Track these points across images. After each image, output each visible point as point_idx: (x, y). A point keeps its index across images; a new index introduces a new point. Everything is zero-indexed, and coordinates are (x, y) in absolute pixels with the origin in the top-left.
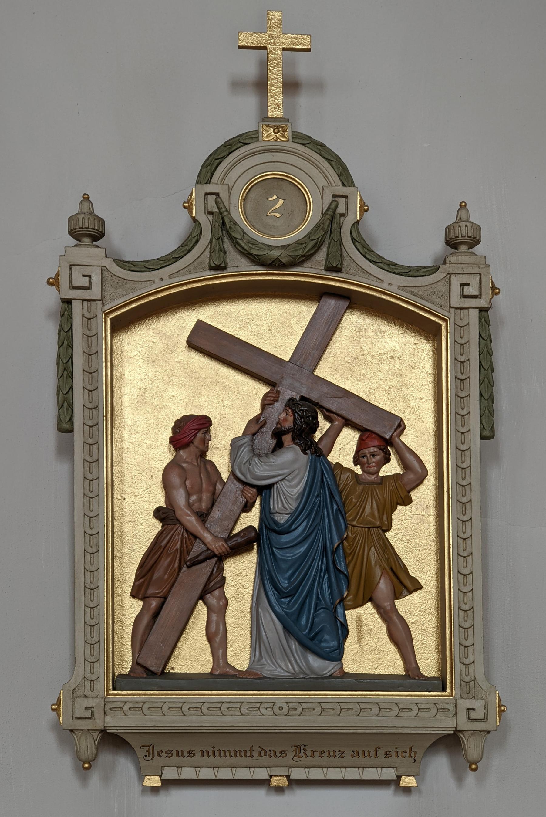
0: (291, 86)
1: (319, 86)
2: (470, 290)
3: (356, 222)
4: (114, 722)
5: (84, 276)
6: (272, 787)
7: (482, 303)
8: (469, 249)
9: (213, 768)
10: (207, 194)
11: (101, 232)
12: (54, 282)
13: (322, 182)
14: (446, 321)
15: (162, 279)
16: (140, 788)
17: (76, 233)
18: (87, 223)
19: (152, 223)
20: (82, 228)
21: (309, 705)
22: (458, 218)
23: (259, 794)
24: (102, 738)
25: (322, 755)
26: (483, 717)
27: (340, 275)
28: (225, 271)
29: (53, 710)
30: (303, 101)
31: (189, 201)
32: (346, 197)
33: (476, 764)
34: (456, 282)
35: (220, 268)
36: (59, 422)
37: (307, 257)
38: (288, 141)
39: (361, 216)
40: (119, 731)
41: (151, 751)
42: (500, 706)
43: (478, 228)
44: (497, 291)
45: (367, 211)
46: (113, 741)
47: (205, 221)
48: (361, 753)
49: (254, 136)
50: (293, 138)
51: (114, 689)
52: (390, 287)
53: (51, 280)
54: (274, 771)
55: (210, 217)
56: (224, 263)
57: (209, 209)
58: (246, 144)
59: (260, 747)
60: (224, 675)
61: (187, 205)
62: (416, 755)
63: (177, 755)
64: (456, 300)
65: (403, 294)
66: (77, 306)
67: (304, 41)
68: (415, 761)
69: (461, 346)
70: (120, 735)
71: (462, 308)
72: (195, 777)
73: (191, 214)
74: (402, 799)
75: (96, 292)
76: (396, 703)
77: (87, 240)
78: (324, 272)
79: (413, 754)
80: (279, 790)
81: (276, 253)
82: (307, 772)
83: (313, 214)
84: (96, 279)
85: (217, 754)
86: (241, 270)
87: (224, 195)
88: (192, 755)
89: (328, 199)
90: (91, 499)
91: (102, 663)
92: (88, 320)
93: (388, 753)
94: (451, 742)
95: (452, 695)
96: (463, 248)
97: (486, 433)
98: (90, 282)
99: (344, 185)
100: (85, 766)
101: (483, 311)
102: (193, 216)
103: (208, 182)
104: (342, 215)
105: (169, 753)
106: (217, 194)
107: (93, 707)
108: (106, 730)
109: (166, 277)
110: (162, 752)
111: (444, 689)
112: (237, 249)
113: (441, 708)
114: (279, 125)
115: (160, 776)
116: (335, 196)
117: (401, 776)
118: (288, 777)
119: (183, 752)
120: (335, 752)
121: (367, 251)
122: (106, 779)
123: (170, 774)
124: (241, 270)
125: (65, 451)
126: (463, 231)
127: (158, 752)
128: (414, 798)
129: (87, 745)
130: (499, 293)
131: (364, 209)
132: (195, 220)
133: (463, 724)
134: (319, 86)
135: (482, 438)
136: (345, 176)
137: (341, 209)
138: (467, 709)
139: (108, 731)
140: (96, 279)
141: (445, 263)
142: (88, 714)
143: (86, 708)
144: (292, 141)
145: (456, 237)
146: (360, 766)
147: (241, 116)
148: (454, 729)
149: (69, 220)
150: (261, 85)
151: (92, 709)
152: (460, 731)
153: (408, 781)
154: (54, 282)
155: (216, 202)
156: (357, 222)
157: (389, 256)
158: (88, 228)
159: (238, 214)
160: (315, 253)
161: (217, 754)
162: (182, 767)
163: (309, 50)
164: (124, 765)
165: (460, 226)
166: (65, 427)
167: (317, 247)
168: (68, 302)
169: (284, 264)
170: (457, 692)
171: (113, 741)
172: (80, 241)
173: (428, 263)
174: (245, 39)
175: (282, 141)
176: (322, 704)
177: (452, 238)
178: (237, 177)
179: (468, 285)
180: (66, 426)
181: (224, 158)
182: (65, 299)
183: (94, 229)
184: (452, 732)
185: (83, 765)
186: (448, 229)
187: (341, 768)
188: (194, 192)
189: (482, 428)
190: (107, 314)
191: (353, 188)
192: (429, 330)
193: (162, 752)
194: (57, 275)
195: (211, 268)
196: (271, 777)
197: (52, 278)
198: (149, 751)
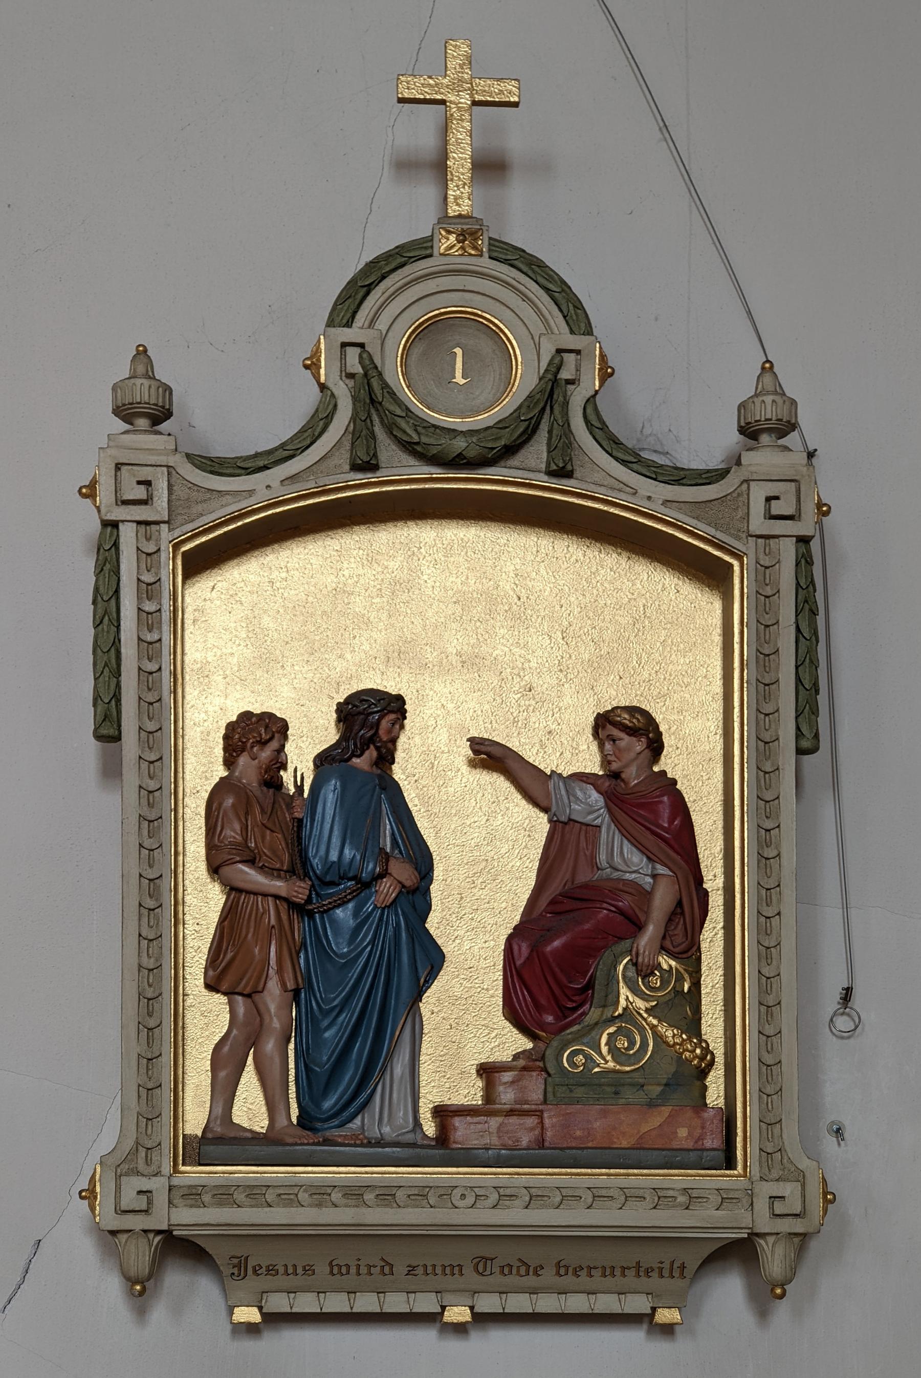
1: (543, 167)
4: (185, 1217)
5: (139, 483)
6: (657, 1324)
7: (804, 528)
8: (779, 438)
9: (318, 1293)
10: (344, 345)
11: (168, 410)
12: (89, 492)
14: (739, 558)
16: (229, 1327)
17: (125, 412)
18: (142, 391)
19: (255, 392)
21: (508, 1192)
23: (635, 1336)
25: (259, 1272)
26: (798, 1212)
27: (572, 482)
28: (378, 474)
31: (316, 353)
32: (578, 352)
33: (141, 1282)
34: (758, 494)
35: (370, 466)
37: (510, 450)
38: (481, 256)
39: (600, 387)
40: (192, 1233)
41: (241, 1268)
43: (168, 390)
46: (179, 1247)
47: (343, 392)
49: (416, 251)
50: (490, 250)
51: (183, 1165)
53: (84, 490)
54: (448, 1298)
55: (351, 383)
56: (552, 464)
57: (350, 370)
59: (383, 1259)
60: (220, 1140)
61: (309, 362)
63: (502, 1272)
64: (758, 524)
65: (670, 514)
67: (510, 91)
69: (764, 600)
70: (191, 1239)
72: (347, 1309)
73: (317, 377)
74: (661, 1347)
76: (589, 1188)
77: (143, 423)
78: (546, 478)
80: (460, 1329)
81: (460, 444)
82: (592, 1301)
83: (524, 379)
84: (161, 487)
86: (403, 473)
87: (373, 348)
92: (148, 558)
93: (307, 1268)
94: (740, 1251)
95: (745, 1176)
96: (765, 439)
97: (805, 744)
100: (141, 1289)
101: (803, 541)
102: (323, 379)
103: (349, 324)
104: (569, 382)
105: (271, 1270)
106: (362, 346)
107: (150, 1192)
109: (275, 484)
111: (730, 1163)
112: (395, 436)
113: (726, 1199)
114: (469, 231)
116: (559, 351)
117: (445, 1307)
118: (472, 1308)
119: (295, 1266)
120: (295, 1266)
121: (612, 444)
123: (489, 1303)
124: (403, 473)
125: (111, 770)
126: (767, 410)
129: (140, 1255)
131: (606, 374)
132: (323, 387)
133: (764, 1224)
134: (543, 167)
135: (800, 752)
138: (770, 1197)
139: (175, 1233)
140: (161, 487)
141: (739, 463)
142: (142, 1204)
144: (490, 258)
145: (756, 421)
146: (501, 1290)
147: (406, 215)
148: (749, 1231)
149: (115, 388)
150: (440, 167)
151: (149, 1194)
152: (757, 1235)
153: (665, 1315)
154: (89, 492)
156: (597, 392)
161: (364, 1270)
163: (516, 105)
164: (205, 1287)
165: (763, 401)
166: (108, 731)
168: (115, 525)
170: (755, 1171)
171: (179, 1247)
172: (132, 424)
173: (714, 462)
175: (470, 255)
176: (475, 1189)
177: (750, 423)
178: (389, 326)
179: (777, 498)
182: (107, 520)
183: (148, 403)
184: (746, 1236)
185: (772, 1290)
186: (742, 406)
187: (559, 1293)
189: (799, 734)
191: (590, 337)
192: (709, 573)
195: (551, 473)
196: (443, 1308)
197: (85, 486)
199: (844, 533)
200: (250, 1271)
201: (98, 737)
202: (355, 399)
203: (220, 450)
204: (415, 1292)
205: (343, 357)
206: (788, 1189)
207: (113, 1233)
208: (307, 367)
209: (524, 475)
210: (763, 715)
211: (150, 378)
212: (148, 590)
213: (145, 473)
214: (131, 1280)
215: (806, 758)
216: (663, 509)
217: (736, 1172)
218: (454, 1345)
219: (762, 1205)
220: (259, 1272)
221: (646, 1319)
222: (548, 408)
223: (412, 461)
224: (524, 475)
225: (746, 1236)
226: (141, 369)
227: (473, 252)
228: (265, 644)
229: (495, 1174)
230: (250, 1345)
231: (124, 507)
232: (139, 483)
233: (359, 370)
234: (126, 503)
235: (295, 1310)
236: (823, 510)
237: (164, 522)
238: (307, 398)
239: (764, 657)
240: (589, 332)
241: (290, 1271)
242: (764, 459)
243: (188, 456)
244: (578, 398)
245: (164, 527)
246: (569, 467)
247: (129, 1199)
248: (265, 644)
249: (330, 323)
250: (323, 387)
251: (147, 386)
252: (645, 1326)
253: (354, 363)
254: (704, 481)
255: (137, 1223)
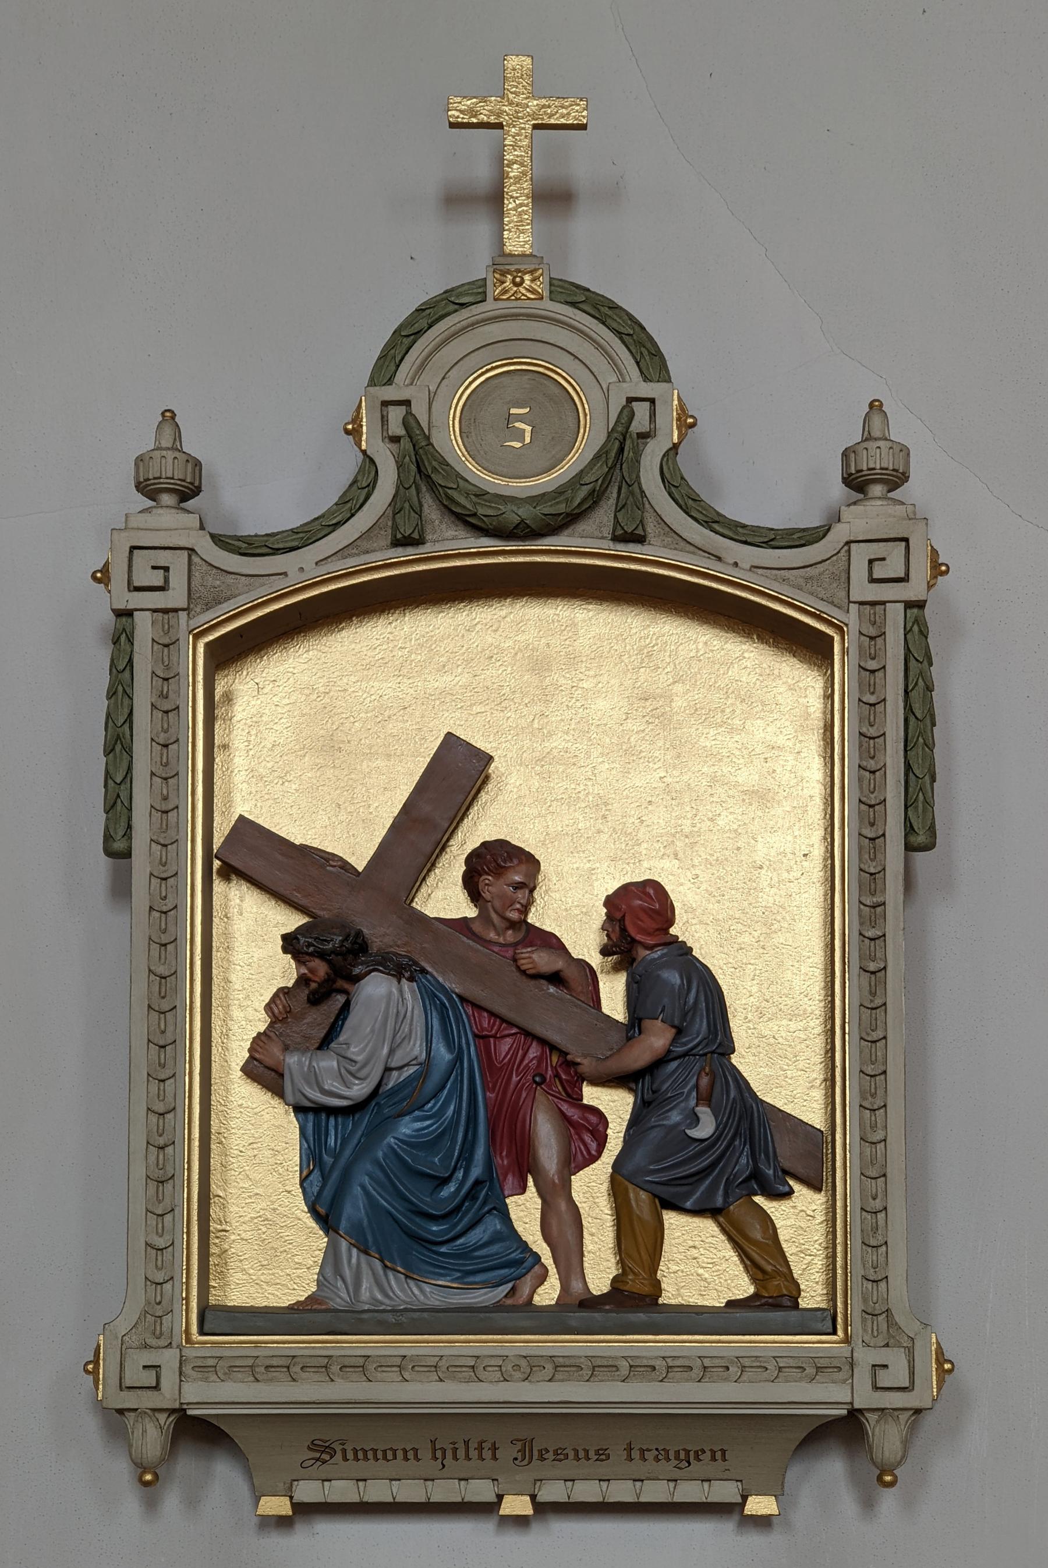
0: (553, 199)
2: (894, 567)
3: (671, 449)
4: (203, 1395)
5: (154, 568)
7: (914, 590)
8: (889, 491)
10: (385, 404)
11: (903, 474)
13: (609, 377)
14: (840, 630)
15: (302, 569)
17: (148, 489)
18: (169, 468)
19: (280, 464)
20: (160, 478)
22: (866, 433)
24: (177, 1423)
29: (87, 1372)
30: (583, 227)
31: (356, 419)
32: (652, 401)
34: (860, 555)
36: (108, 838)
39: (682, 437)
42: (940, 1362)
43: (197, 464)
44: (943, 568)
45: (693, 426)
48: (400, 1454)
49: (478, 291)
52: (740, 571)
55: (394, 447)
58: (463, 305)
62: (444, 1458)
64: (862, 590)
66: (143, 624)
67: (576, 113)
68: (444, 1466)
69: (869, 675)
71: (873, 604)
73: (359, 446)
74: (755, 1539)
75: (176, 596)
78: (611, 543)
79: (439, 1454)
81: (525, 512)
85: (350, 1455)
86: (454, 547)
87: (419, 410)
88: (562, 1457)
89: (617, 403)
90: (163, 981)
91: (177, 1284)
96: (877, 490)
97: (921, 839)
98: (166, 580)
99: (646, 379)
100: (149, 1479)
101: (917, 605)
102: (363, 448)
103: (390, 381)
104: (644, 436)
105: (560, 1455)
106: (407, 403)
108: (185, 1410)
110: (548, 1451)
113: (820, 1368)
115: (291, 1498)
116: (630, 400)
117: (503, 1496)
118: (533, 1497)
119: (587, 1451)
120: (587, 1451)
121: (690, 503)
122: (192, 1503)
125: (121, 889)
126: (877, 458)
127: (540, 1451)
128: (775, 1538)
129: (151, 1438)
130: (947, 572)
132: (364, 452)
133: (864, 1398)
134: (612, 195)
135: (909, 848)
136: (650, 359)
137: (640, 422)
138: (874, 1366)
139: (190, 1412)
143: (145, 1367)
144: (551, 300)
148: (850, 1407)
153: (760, 1505)
154: (103, 576)
155: (405, 424)
156: (675, 447)
157: (731, 510)
158: (172, 478)
159: (452, 443)
160: (591, 508)
162: (433, 1480)
163: (583, 127)
164: (224, 1475)
167: (595, 499)
168: (128, 613)
169: (532, 530)
171: (199, 1431)
173: (813, 520)
174: (460, 108)
175: (529, 299)
180: (119, 845)
181: (419, 334)
184: (845, 1412)
186: (139, 460)
187: (635, 1480)
188: (363, 404)
189: (909, 829)
190: (197, 637)
192: (808, 644)
193: (548, 1451)
194: (106, 565)
198: (523, 1451)
199: (957, 599)
200: (536, 1453)
201: (109, 853)
202: (400, 466)
203: (248, 529)
204: (365, 1480)
205: (384, 420)
206: (897, 1360)
207: (121, 1412)
208: (347, 432)
209: (586, 545)
210: (870, 808)
211: (177, 449)
212: (168, 678)
213: (163, 558)
214: (141, 1467)
215: (919, 857)
216: (748, 576)
217: (194, 1328)
218: (513, 1539)
219: (862, 1377)
220: (545, 1456)
221: (737, 1509)
222: (618, 466)
223: (461, 532)
224: (586, 545)
225: (845, 1412)
226: (166, 443)
227: (532, 296)
228: (312, 743)
229: (338, 1342)
230: (278, 1542)
231: (136, 593)
232: (154, 568)
233: (401, 431)
234: (138, 589)
235: (643, 1499)
236: (938, 569)
237: (183, 610)
238: (345, 467)
239: (869, 742)
240: (668, 380)
241: (582, 1454)
242: (870, 516)
243: (213, 536)
244: (651, 456)
245: (183, 615)
246: (640, 531)
247: (135, 1375)
248: (312, 743)
249: (372, 382)
250: (364, 452)
251: (170, 460)
252: (736, 1517)
253: (396, 428)
254: (797, 543)
255: (147, 1400)
